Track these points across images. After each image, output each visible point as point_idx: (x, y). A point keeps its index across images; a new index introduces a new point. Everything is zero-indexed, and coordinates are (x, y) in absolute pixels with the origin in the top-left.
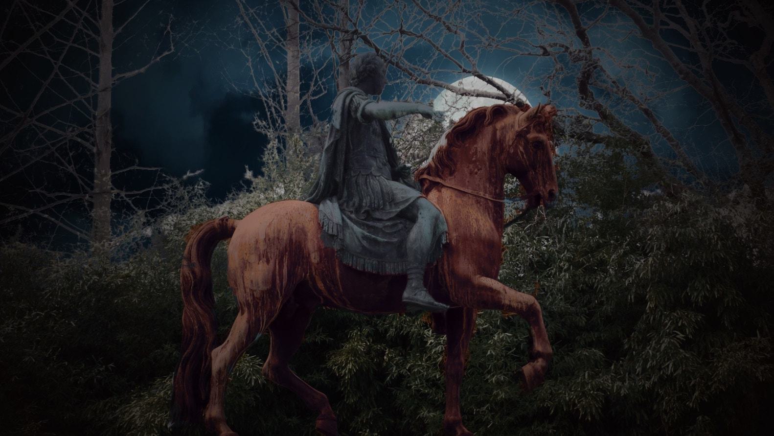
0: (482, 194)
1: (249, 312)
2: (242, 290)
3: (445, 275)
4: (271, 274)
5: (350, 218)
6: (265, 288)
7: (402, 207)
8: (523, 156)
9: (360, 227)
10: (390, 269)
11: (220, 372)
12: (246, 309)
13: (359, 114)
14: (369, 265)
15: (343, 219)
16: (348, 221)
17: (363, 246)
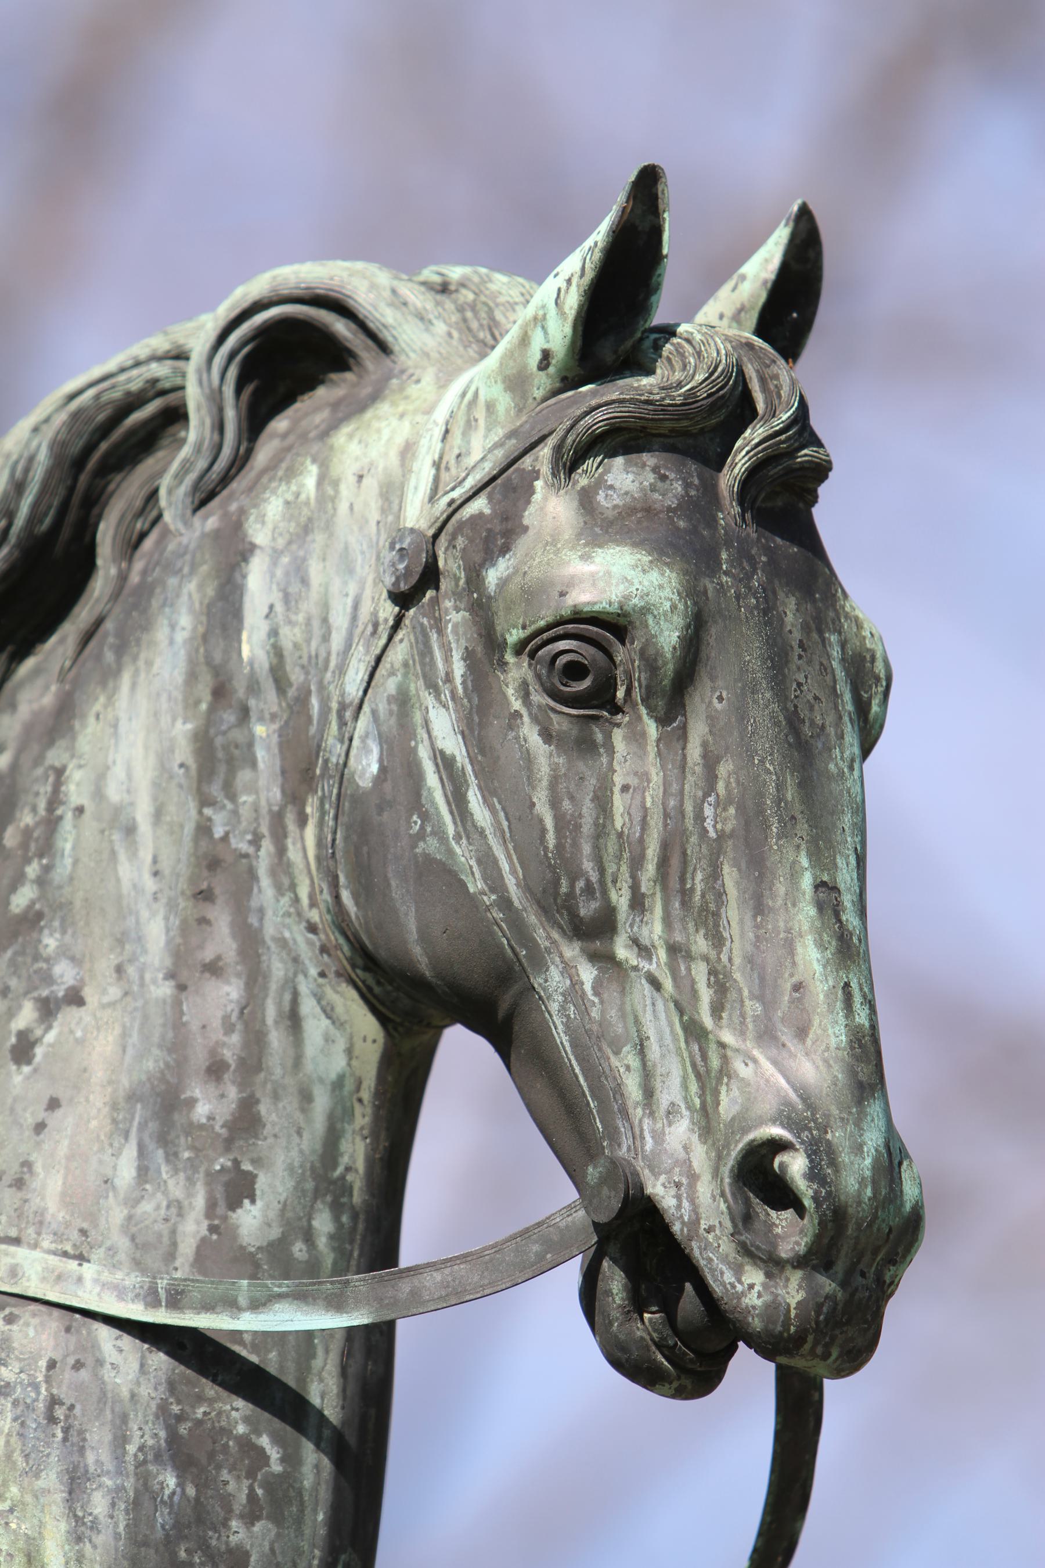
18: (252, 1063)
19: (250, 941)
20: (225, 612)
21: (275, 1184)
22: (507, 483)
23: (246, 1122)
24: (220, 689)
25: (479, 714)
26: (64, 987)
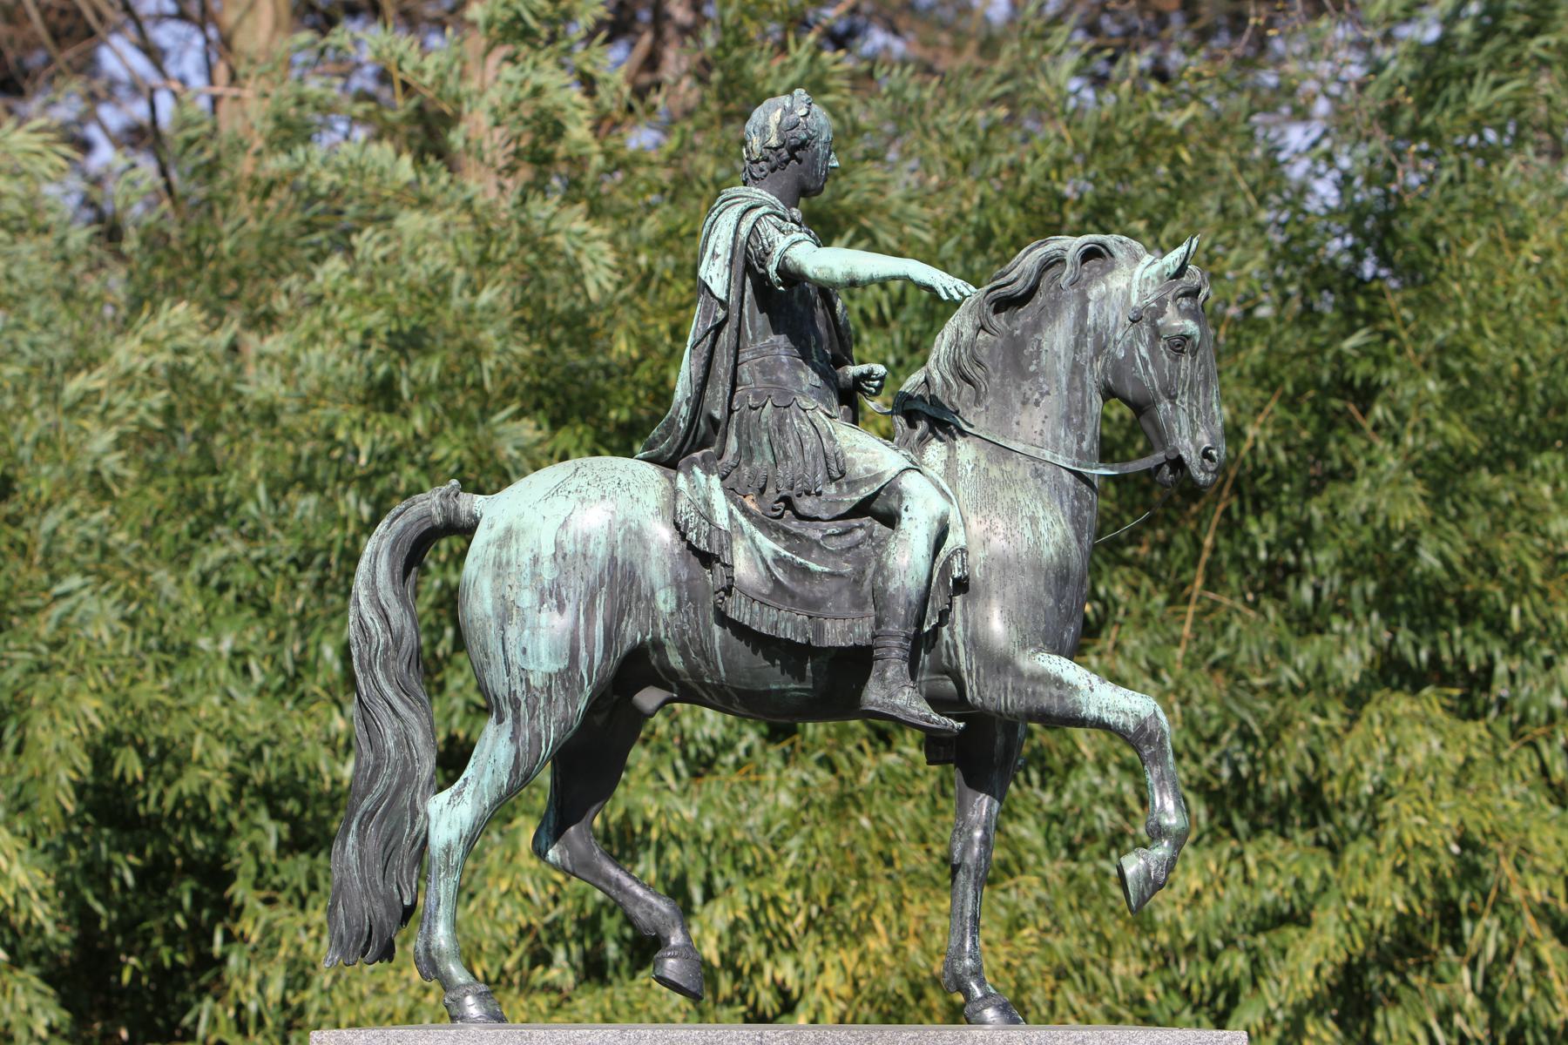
0: (1047, 454)
1: (517, 720)
2: (502, 667)
3: (956, 647)
4: (568, 636)
5: (745, 511)
6: (554, 667)
7: (865, 491)
8: (1145, 367)
9: (769, 536)
10: (836, 634)
11: (448, 850)
12: (508, 710)
13: (772, 269)
14: (787, 624)
15: (731, 513)
16: (742, 519)
17: (777, 581)
18: (1083, 411)
19: (1083, 384)
20: (1083, 312)
21: (1088, 437)
22: (1162, 302)
23: (1083, 424)
24: (1081, 330)
25: (1152, 349)
26: (1471, 437)
